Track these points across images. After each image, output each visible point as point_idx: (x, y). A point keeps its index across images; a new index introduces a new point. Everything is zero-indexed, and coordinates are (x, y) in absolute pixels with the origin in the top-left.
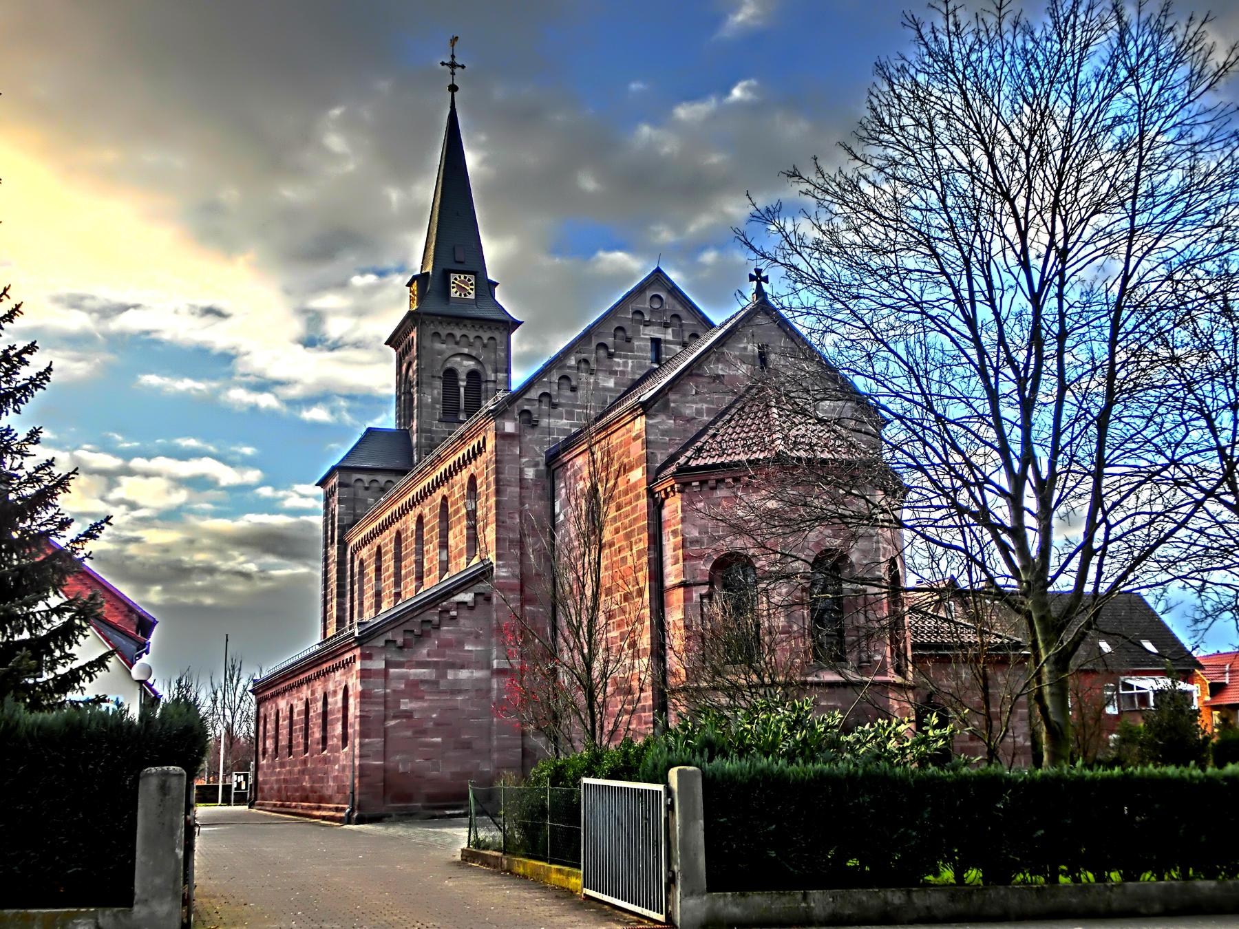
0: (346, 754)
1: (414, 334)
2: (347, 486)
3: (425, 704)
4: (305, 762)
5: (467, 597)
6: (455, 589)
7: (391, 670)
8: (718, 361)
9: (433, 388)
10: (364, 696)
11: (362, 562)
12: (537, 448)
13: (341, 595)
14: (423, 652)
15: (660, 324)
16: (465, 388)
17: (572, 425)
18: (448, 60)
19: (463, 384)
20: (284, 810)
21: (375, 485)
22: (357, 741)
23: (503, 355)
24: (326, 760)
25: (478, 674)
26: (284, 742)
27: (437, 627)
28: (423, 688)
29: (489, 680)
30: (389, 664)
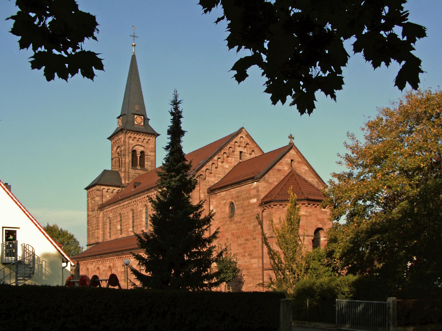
8: (279, 164)
17: (215, 180)
18: (132, 34)
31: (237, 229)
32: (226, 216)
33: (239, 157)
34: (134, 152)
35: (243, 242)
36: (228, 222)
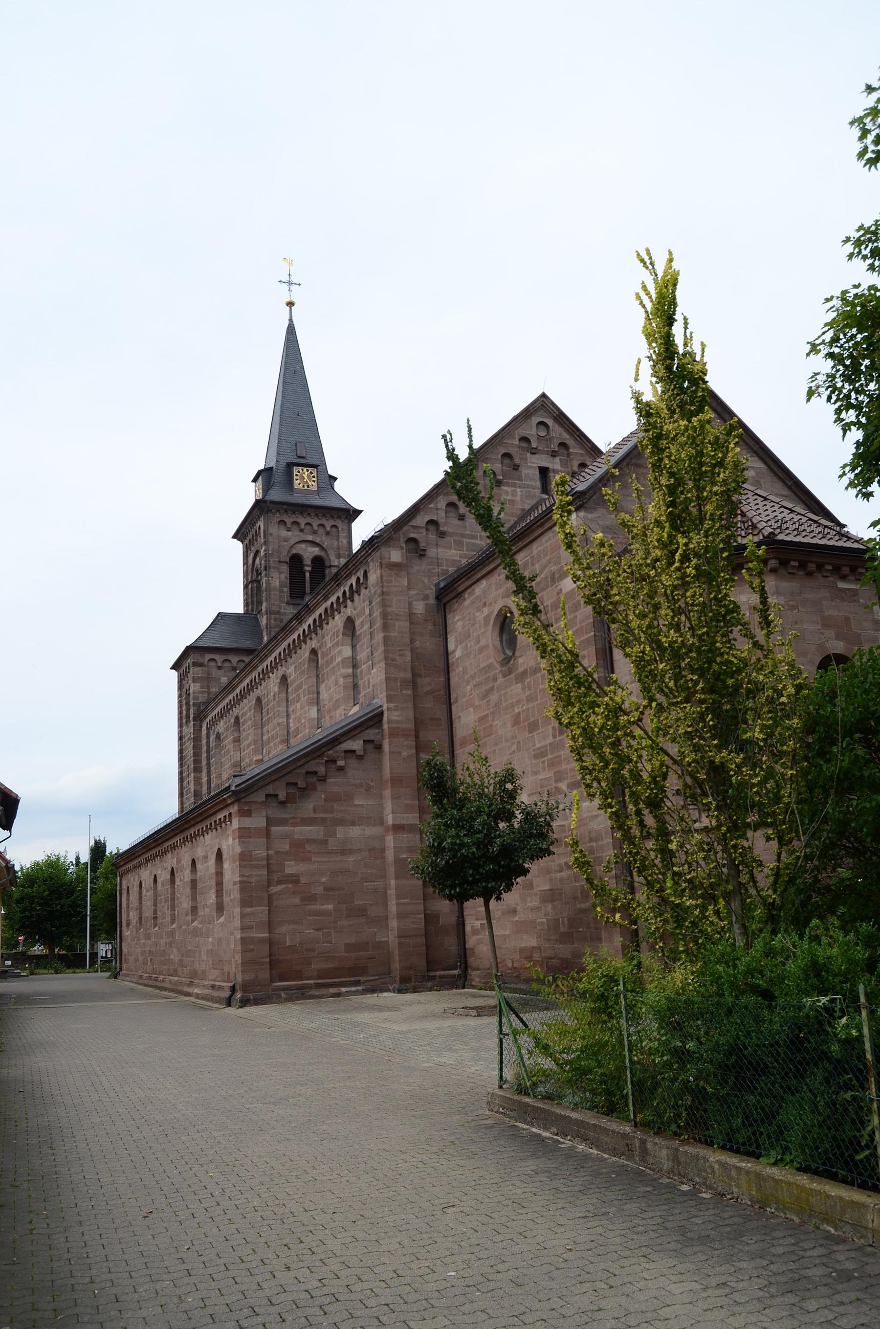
0: (221, 925)
1: (261, 523)
2: (201, 665)
3: (313, 867)
4: (172, 933)
5: (356, 745)
6: (343, 735)
7: (273, 829)
9: (280, 573)
10: (245, 859)
11: (218, 736)
12: (426, 580)
13: (198, 770)
14: (307, 807)
15: (547, 453)
16: (311, 573)
19: (308, 569)
20: (150, 983)
21: (227, 664)
22: (237, 910)
23: (345, 541)
24: (195, 933)
25: (370, 831)
26: (148, 912)
27: (323, 779)
28: (308, 847)
29: (382, 839)
30: (270, 822)
31: (529, 699)
32: (492, 660)
33: (538, 484)
34: (296, 561)
35: (550, 740)
36: (501, 680)
